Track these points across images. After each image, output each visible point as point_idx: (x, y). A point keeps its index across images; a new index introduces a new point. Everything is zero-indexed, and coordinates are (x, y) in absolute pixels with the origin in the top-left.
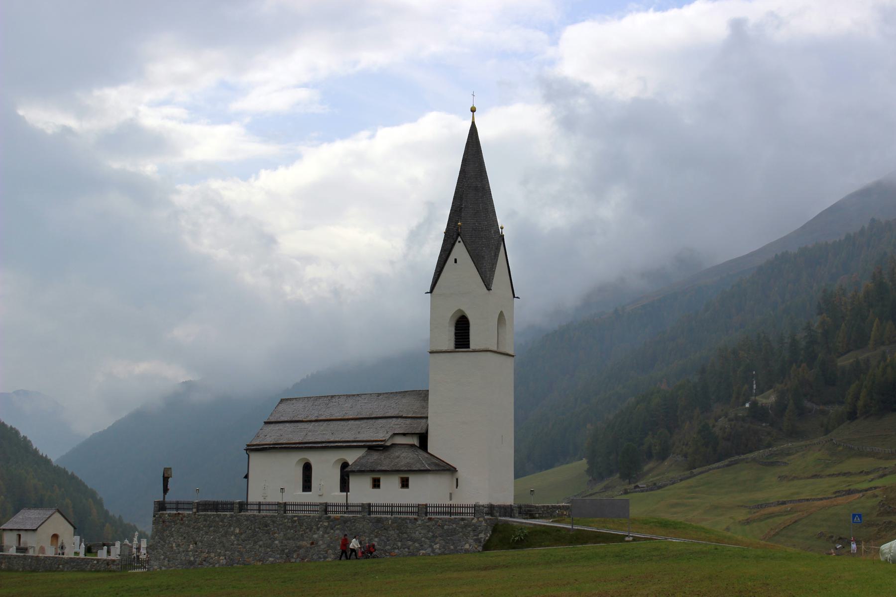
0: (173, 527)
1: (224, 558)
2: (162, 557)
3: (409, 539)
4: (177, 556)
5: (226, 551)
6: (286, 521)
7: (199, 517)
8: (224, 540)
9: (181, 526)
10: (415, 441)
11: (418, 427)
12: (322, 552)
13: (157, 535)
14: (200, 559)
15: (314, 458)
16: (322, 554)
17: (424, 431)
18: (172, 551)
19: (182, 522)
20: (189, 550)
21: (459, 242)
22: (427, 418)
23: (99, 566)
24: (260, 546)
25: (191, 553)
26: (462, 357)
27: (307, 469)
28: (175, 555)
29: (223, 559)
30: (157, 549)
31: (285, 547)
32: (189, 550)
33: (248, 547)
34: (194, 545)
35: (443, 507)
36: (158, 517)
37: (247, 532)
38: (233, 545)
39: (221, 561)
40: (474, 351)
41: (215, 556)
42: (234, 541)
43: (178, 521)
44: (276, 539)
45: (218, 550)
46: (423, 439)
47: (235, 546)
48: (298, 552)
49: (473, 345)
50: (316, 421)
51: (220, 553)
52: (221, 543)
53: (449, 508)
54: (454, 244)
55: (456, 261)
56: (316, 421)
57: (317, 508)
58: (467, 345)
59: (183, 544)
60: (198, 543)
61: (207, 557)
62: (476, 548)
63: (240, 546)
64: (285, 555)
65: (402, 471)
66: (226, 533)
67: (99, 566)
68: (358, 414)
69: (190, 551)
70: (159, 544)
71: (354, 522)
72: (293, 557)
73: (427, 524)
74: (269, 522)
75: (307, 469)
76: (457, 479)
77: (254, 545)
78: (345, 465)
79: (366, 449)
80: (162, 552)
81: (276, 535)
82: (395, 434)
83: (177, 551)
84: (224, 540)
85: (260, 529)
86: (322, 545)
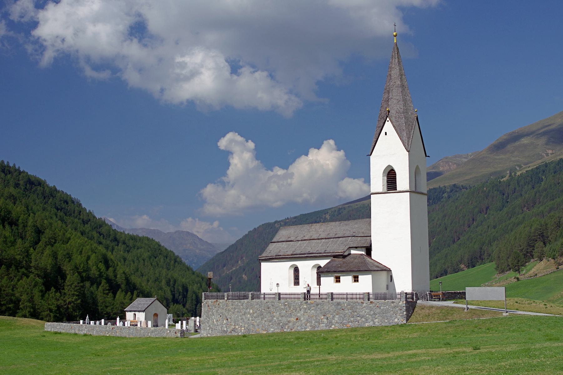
2: (208, 328)
6: (280, 305)
7: (229, 303)
15: (300, 264)
20: (224, 323)
21: (388, 121)
22: (371, 236)
25: (225, 325)
26: (392, 196)
36: (205, 303)
42: (250, 318)
46: (369, 251)
49: (399, 189)
60: (228, 319)
69: (224, 324)
73: (370, 306)
76: (391, 276)
77: (261, 321)
83: (217, 324)
84: (244, 317)
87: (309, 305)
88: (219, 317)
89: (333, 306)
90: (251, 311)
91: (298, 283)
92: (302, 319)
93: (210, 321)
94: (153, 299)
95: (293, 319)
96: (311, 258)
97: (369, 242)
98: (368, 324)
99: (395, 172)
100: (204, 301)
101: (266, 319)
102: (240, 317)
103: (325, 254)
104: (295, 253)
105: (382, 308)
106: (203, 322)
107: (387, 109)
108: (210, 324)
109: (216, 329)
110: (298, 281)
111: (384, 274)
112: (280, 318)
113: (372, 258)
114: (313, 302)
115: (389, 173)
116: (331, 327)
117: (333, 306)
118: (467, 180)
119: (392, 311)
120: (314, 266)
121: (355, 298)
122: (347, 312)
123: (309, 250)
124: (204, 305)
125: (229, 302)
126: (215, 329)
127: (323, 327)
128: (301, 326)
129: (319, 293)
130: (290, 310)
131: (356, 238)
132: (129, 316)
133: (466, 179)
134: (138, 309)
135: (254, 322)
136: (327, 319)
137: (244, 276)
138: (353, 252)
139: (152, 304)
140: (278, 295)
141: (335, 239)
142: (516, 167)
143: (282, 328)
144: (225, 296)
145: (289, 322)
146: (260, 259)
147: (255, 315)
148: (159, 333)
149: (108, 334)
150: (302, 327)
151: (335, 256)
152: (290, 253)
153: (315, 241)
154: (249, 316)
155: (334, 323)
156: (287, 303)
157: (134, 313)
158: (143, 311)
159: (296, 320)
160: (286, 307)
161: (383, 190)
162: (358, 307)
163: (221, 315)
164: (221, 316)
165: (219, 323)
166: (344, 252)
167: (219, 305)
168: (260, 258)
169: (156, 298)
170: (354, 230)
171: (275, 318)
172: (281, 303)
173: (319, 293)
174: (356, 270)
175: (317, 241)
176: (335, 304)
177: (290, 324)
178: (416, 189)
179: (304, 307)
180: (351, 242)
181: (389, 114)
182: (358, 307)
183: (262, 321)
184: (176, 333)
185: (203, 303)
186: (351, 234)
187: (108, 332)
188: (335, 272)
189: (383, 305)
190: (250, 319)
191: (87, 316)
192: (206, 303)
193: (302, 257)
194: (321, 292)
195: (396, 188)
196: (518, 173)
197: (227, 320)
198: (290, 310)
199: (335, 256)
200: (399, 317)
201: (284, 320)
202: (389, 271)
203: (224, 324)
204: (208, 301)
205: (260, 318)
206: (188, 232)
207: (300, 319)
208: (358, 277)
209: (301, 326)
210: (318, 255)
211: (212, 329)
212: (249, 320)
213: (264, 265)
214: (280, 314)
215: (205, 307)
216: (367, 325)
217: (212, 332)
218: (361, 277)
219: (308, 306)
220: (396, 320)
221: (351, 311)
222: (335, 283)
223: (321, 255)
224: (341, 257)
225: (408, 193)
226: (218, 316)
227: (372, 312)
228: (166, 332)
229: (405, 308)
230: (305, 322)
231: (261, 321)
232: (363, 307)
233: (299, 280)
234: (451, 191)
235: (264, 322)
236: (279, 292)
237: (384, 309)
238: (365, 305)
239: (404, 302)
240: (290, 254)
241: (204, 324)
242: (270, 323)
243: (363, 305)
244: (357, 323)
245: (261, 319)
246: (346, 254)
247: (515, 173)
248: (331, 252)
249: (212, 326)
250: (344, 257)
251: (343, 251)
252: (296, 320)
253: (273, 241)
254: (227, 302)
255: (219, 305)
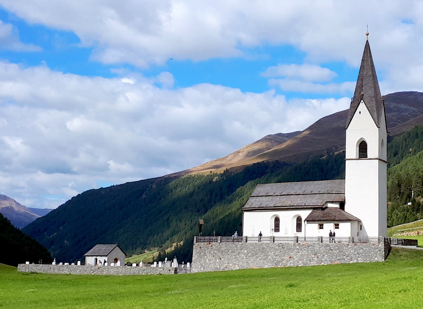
0: (206, 251)
1: (238, 266)
2: (200, 266)
3: (344, 255)
4: (209, 266)
5: (239, 262)
6: (275, 246)
7: (222, 245)
8: (238, 256)
9: (211, 250)
10: (337, 206)
11: (338, 198)
12: (296, 262)
13: (196, 255)
14: (223, 267)
15: (281, 214)
16: (296, 263)
17: (343, 201)
18: (206, 263)
19: (212, 247)
20: (217, 262)
21: (362, 103)
22: (344, 193)
23: (164, 271)
24: (260, 259)
25: (217, 264)
26: (363, 162)
27: (277, 220)
28: (208, 265)
29: (237, 267)
30: (196, 262)
31: (275, 260)
32: (217, 262)
33: (252, 260)
34: (220, 260)
35: (341, 238)
36: (197, 246)
37: (252, 252)
38: (243, 259)
39: (236, 268)
40: (371, 159)
41: (232, 265)
42: (244, 257)
43: (209, 247)
44: (269, 255)
45: (234, 262)
46: (342, 205)
47: (245, 259)
48: (282, 262)
49: (369, 157)
50: (287, 195)
51: (236, 263)
52: (236, 258)
53: (348, 239)
54: (359, 104)
55: (360, 113)
56: (287, 195)
57: (293, 239)
58: (366, 156)
59: (212, 259)
60: (221, 259)
61: (228, 266)
62: (381, 260)
63: (248, 260)
64: (275, 264)
65: (336, 220)
66: (239, 253)
67: (164, 271)
68: (304, 192)
69: (217, 263)
70: (197, 260)
71: (314, 246)
72: (279, 265)
73: (354, 247)
74: (265, 247)
75: (277, 220)
76: (361, 225)
77: (256, 259)
78: (299, 219)
79: (312, 209)
80: (200, 264)
81: (269, 253)
82: (327, 202)
83: (209, 263)
84: (238, 256)
85: (259, 250)
86: (296, 258)
87: (302, 246)
88: (212, 257)
89: (323, 247)
90: (246, 251)
91: (278, 230)
92: (295, 257)
93: (202, 260)
94: (115, 245)
95: (287, 258)
96: (279, 210)
97: (344, 198)
98: (353, 261)
99: (366, 144)
100: (196, 244)
101: (260, 258)
102: (233, 257)
103: (305, 207)
104: (276, 205)
105: (365, 249)
106: (195, 261)
107: (362, 93)
108: (201, 263)
109: (208, 267)
110: (278, 228)
111: (356, 224)
112: (275, 257)
113: (345, 210)
114: (305, 244)
115: (361, 143)
116: (321, 264)
117: (323, 247)
118: (288, 157)
119: (373, 251)
120: (295, 216)
121: (348, 241)
122: (334, 252)
123: (290, 204)
124: (195, 247)
125: (222, 244)
126: (207, 267)
127: (314, 263)
128: (294, 263)
129: (305, 237)
130: (284, 250)
131: (331, 194)
132: (90, 260)
133: (287, 156)
134: (101, 254)
135: (248, 261)
136: (318, 257)
137: (66, 241)
138: (330, 205)
139: (114, 250)
140: (273, 238)
141: (312, 195)
142: (333, 148)
143: (276, 264)
144: (219, 240)
145: (283, 260)
146: (243, 210)
147: (249, 255)
148: (151, 271)
149: (93, 273)
150: (294, 264)
151: (314, 209)
152: (272, 205)
153: (294, 196)
154: (243, 255)
155: (324, 260)
156: (281, 245)
157: (95, 257)
158: (106, 256)
159: (290, 258)
160: (281, 247)
161: (356, 157)
162: (345, 248)
163: (213, 255)
164: (213, 256)
165: (211, 262)
166: (323, 205)
167: (212, 246)
168: (243, 209)
169: (117, 245)
170: (328, 188)
171: (270, 257)
172: (275, 245)
173: (305, 237)
174: (338, 219)
175: (296, 196)
176: (325, 246)
177: (284, 262)
178: (348, 160)
179: (297, 247)
180: (326, 198)
181: (363, 97)
182: (345, 248)
183: (256, 260)
184: (170, 271)
185: (195, 245)
186: (326, 191)
187: (93, 271)
188: (320, 221)
189: (365, 247)
190: (245, 258)
191: (55, 260)
192: (198, 245)
193: (284, 209)
194: (306, 236)
195: (367, 156)
196: (336, 153)
197: (220, 259)
198: (284, 250)
199: (314, 209)
200: (378, 256)
201: (278, 259)
202: (359, 221)
203: (217, 263)
204: (200, 244)
205: (255, 257)
206: (5, 196)
207: (293, 258)
208: (338, 225)
209: (294, 263)
210: (300, 207)
211: (204, 267)
212: (243, 259)
213: (247, 215)
214: (274, 253)
215: (196, 249)
216: (351, 262)
217: (204, 270)
218: (341, 225)
219: (300, 247)
220: (376, 259)
221: (338, 251)
222: (319, 230)
223: (302, 207)
224: (321, 209)
225: (378, 160)
226: (211, 256)
227: (356, 253)
228: (159, 270)
229: (383, 249)
230: (298, 260)
231: (256, 259)
232: (349, 248)
233: (297, 224)
234: (273, 167)
235: (258, 260)
236: (274, 236)
237: (366, 250)
238: (350, 246)
239: (383, 245)
240: (272, 206)
241: (195, 263)
242: (265, 261)
243: (349, 246)
244: (343, 260)
245: (256, 258)
246: (324, 207)
247: (333, 154)
248: (295, 205)
249: (204, 264)
250: (323, 209)
251: (322, 204)
252: (290, 258)
253: (252, 195)
254: (221, 244)
255: (212, 246)
